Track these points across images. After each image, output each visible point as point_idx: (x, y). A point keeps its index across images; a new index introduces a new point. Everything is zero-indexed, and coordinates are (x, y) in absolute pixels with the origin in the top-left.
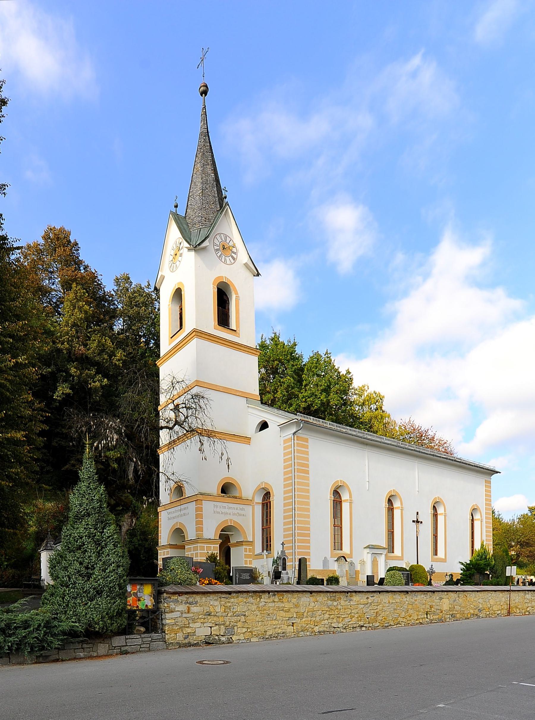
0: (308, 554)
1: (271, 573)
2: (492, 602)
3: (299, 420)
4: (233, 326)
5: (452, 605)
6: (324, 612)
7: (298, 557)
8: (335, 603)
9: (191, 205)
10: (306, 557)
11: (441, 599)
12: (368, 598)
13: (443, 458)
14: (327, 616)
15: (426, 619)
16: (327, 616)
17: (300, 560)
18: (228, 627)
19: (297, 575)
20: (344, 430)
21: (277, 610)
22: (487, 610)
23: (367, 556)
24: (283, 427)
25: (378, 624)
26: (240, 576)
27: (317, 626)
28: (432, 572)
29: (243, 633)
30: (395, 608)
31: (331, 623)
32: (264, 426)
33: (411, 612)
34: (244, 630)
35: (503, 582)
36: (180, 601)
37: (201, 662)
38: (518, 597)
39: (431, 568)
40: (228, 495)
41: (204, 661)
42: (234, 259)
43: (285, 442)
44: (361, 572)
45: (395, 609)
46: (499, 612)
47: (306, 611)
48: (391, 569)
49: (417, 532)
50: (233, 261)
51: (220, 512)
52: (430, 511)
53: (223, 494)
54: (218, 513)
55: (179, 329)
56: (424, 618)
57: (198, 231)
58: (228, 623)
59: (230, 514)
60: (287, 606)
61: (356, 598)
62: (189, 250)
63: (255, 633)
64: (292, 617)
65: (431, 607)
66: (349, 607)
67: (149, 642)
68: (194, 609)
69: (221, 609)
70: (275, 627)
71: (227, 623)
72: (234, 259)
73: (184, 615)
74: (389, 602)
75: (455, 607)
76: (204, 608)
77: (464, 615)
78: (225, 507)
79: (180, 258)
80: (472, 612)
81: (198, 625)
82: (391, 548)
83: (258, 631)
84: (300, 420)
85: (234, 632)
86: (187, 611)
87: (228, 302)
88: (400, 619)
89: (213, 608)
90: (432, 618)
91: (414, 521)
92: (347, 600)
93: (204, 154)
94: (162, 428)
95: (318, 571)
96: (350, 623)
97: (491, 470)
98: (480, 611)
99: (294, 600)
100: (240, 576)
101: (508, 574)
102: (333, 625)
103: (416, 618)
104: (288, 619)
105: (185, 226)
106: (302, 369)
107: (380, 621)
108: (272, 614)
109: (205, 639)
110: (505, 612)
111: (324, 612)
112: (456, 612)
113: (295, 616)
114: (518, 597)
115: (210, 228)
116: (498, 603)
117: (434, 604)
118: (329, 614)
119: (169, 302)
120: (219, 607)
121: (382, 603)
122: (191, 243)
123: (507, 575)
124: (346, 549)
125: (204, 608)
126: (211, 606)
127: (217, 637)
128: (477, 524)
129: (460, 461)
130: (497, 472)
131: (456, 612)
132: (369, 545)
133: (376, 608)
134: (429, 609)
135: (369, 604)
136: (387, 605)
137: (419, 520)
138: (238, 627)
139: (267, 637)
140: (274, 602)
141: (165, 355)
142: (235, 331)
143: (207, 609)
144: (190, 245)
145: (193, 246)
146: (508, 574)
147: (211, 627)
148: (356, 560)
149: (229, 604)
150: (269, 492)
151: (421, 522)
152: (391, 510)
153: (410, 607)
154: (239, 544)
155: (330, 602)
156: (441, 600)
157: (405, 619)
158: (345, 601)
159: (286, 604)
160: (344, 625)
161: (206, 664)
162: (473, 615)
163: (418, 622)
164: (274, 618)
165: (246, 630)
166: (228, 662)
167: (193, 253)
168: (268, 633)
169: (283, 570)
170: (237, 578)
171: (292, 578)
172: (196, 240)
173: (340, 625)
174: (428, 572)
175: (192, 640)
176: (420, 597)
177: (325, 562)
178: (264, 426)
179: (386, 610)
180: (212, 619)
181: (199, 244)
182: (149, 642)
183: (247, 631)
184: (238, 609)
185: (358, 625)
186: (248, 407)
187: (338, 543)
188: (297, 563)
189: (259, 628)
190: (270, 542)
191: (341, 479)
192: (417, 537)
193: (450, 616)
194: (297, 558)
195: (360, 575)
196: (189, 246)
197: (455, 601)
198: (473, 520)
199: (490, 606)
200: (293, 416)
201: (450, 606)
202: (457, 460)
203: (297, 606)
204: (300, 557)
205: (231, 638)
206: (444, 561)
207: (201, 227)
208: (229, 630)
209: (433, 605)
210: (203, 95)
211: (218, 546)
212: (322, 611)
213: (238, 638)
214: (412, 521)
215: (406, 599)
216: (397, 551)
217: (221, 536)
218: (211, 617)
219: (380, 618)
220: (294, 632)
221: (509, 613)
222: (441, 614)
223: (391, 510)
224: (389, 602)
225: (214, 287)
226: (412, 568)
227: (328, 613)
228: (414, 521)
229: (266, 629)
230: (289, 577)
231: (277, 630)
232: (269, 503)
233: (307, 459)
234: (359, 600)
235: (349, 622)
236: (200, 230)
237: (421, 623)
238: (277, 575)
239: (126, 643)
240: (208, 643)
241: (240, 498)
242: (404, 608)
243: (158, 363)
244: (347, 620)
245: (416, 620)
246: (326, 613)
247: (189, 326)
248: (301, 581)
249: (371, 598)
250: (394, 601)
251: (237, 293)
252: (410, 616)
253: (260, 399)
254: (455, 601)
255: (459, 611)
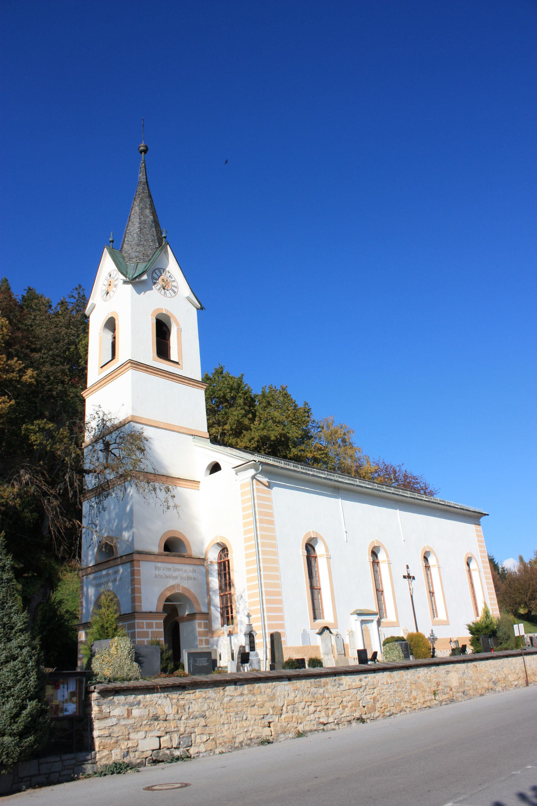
0: (282, 626)
1: (236, 656)
2: (506, 670)
3: (257, 461)
4: (174, 356)
5: (461, 679)
6: (308, 703)
7: (268, 632)
8: (321, 690)
9: (128, 241)
10: (279, 631)
11: (448, 672)
12: (361, 680)
13: (425, 500)
14: (312, 708)
15: (435, 701)
16: (312, 708)
17: (272, 636)
18: (183, 736)
19: (269, 657)
20: (311, 473)
21: (247, 705)
22: (502, 682)
23: (355, 623)
24: (238, 469)
25: (377, 714)
26: (195, 661)
27: (300, 723)
28: (434, 639)
29: (204, 742)
30: (396, 689)
31: (319, 718)
32: (215, 468)
33: (414, 693)
34: (205, 738)
35: (513, 645)
36: (117, 702)
37: (149, 789)
38: (533, 661)
39: (432, 635)
40: (174, 553)
41: (153, 786)
42: (175, 292)
43: (243, 486)
44: (350, 647)
45: (395, 691)
46: (516, 683)
47: (286, 705)
48: (387, 642)
49: (410, 589)
50: (173, 294)
51: (164, 576)
52: (422, 563)
53: (167, 553)
54: (161, 577)
55: (111, 359)
56: (432, 700)
57: (135, 265)
58: (182, 730)
59: (176, 578)
60: (260, 699)
61: (346, 680)
62: (125, 282)
63: (220, 742)
64: (267, 714)
65: (438, 684)
66: (339, 694)
67: (72, 766)
68: (136, 712)
69: (173, 710)
70: (245, 730)
71: (181, 730)
72: (175, 292)
73: (123, 722)
74: (387, 683)
75: (466, 681)
76: (149, 711)
77: (477, 690)
78: (169, 569)
79: (114, 289)
80: (486, 685)
81: (141, 734)
82: (381, 613)
83: (224, 738)
84: (259, 461)
85: (192, 741)
86: (126, 715)
87: (168, 333)
88: (403, 705)
89: (162, 709)
90: (441, 699)
91: (404, 577)
92: (335, 685)
93: (143, 199)
94: (88, 472)
95: (297, 650)
96: (343, 716)
97: (478, 513)
98: (495, 683)
99: (268, 691)
100: (195, 661)
101: (517, 634)
102: (321, 720)
103: (422, 701)
104: (263, 718)
105: (121, 260)
106: (253, 400)
107: (379, 709)
108: (241, 711)
109: (151, 755)
110: (522, 682)
111: (308, 703)
112: (468, 688)
113: (271, 712)
114: (533, 661)
115: (148, 264)
116: (513, 671)
117: (440, 680)
118: (315, 706)
119: (100, 331)
120: (170, 707)
121: (379, 684)
122: (127, 276)
123: (516, 635)
124: (328, 618)
125: (149, 711)
126: (159, 707)
127: (168, 752)
128: (475, 575)
129: (443, 503)
130: (485, 515)
131: (468, 688)
132: (357, 610)
133: (372, 692)
134: (436, 688)
135: (363, 688)
136: (386, 686)
137: (411, 575)
138: (197, 734)
139: (237, 745)
140: (242, 694)
141: (93, 386)
142: (177, 363)
143: (153, 711)
144: (126, 277)
145: (129, 279)
146: (517, 634)
147: (159, 737)
148: (342, 630)
149: (184, 702)
150: (227, 548)
151: (414, 578)
152: (375, 563)
153: (414, 686)
154: (192, 616)
155: (313, 690)
156: (448, 674)
157: (409, 704)
158: (334, 686)
159: (258, 696)
160: (335, 719)
161: (157, 790)
162: (488, 689)
163: (425, 706)
164: (245, 718)
165: (208, 738)
166: (186, 785)
167: (130, 286)
168: (238, 740)
169: (251, 651)
170: (191, 665)
171: (263, 660)
172: (132, 274)
173: (331, 720)
174: (429, 639)
175: (133, 758)
176: (422, 671)
177: (305, 635)
178: (215, 468)
179: (384, 693)
180: (159, 727)
181: (136, 278)
182: (72, 766)
183: (209, 739)
184: (195, 708)
185: (353, 718)
186: (195, 445)
187: (316, 614)
188: (268, 640)
189: (226, 733)
190: (232, 613)
191: (314, 530)
192: (412, 596)
193: (462, 693)
194: (268, 633)
195: (349, 649)
196: (124, 278)
197: (464, 673)
198: (469, 571)
199: (504, 676)
200: (248, 457)
201: (460, 681)
202: (441, 503)
203: (272, 698)
204: (272, 631)
205: (188, 750)
206: (446, 623)
207: (138, 261)
208: (184, 739)
209: (440, 682)
210: (143, 153)
211: (162, 621)
212: (307, 702)
213: (197, 750)
214: (402, 577)
215: (406, 677)
216: (391, 615)
217: (166, 608)
218: (159, 722)
219: (378, 705)
220: (272, 735)
221: (527, 684)
222: (451, 692)
223: (375, 563)
224: (387, 683)
225: (152, 319)
226: (411, 637)
227: (313, 703)
228: (404, 577)
229: (235, 734)
230: (259, 659)
231: (249, 734)
232: (227, 562)
233: (270, 507)
234: (350, 683)
235: (341, 714)
236: (137, 265)
237: (430, 707)
238: (244, 658)
239: (39, 770)
240: (155, 762)
241: (191, 557)
242: (406, 689)
243: (84, 394)
244: (338, 712)
245: (423, 704)
246: (311, 705)
247: (122, 356)
248: (275, 664)
249: (364, 679)
250: (393, 681)
251: (178, 324)
252: (415, 699)
253: (208, 436)
254: (464, 673)
255: (471, 686)
